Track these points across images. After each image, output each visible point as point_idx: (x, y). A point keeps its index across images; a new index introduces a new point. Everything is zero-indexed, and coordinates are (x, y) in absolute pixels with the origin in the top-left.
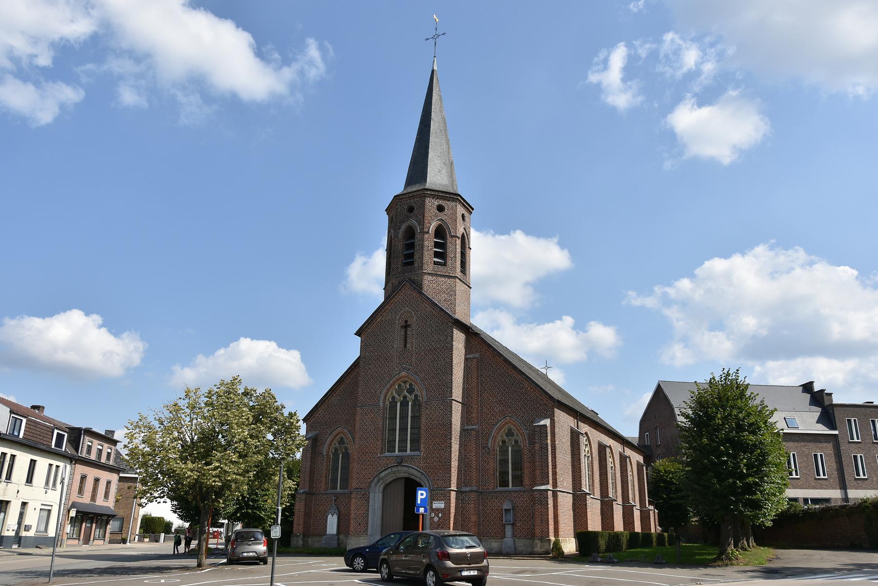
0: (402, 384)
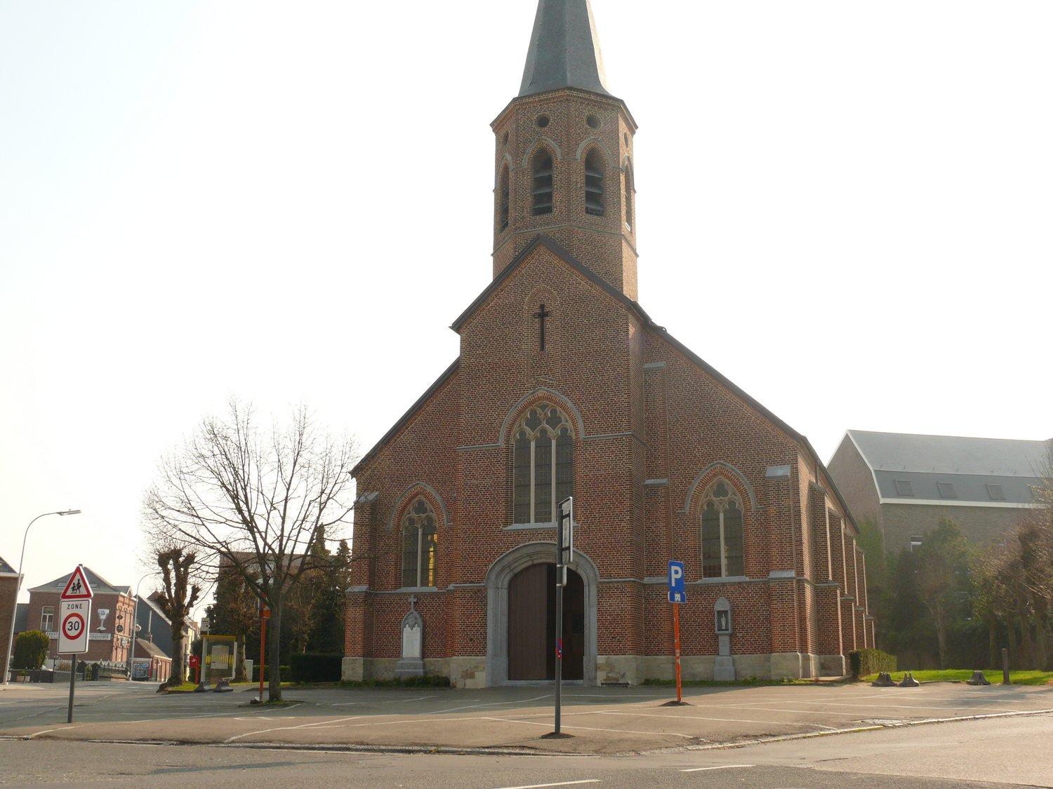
0: (539, 411)
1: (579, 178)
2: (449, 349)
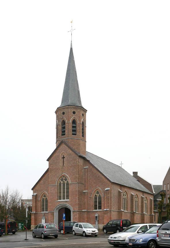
1: (71, 125)
2: (46, 166)
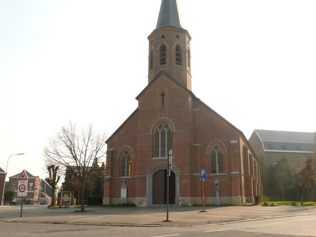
1: (174, 53)
2: (135, 105)
